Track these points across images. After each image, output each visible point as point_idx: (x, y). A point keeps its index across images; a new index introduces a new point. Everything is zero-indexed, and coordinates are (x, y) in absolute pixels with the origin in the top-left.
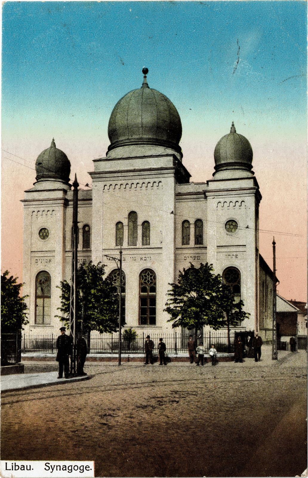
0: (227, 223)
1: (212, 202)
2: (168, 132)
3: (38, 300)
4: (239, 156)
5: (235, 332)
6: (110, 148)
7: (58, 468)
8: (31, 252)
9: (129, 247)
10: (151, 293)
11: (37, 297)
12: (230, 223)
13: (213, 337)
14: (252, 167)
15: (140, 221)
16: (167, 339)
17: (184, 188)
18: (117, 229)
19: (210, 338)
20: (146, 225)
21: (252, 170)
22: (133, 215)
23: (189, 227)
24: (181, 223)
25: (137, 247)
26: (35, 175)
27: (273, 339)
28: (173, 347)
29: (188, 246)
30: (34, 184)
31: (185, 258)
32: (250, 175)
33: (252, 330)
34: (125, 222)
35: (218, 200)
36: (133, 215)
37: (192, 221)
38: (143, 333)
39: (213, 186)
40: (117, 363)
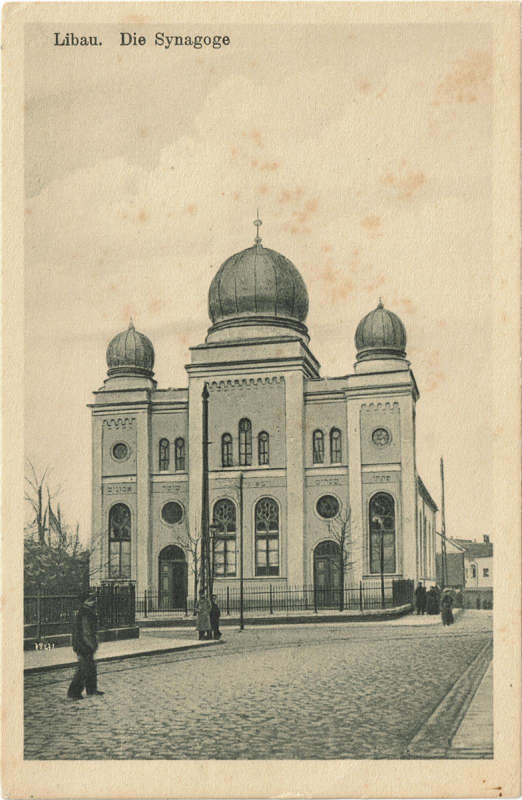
0: (373, 433)
1: (354, 406)
2: (287, 303)
3: (112, 544)
4: (384, 341)
5: (393, 581)
6: (211, 331)
7: (207, 41)
8: (136, 475)
9: (178, 472)
10: (229, 533)
11: (110, 540)
12: (379, 432)
13: (275, 591)
14: (153, 374)
15: (255, 433)
16: (365, 590)
17: (312, 387)
18: (224, 443)
19: (361, 589)
20: (263, 437)
21: (154, 378)
22: (245, 424)
23: (230, 442)
24: (157, 443)
25: (252, 467)
26: (106, 369)
27: (196, 599)
28: (238, 607)
29: (166, 472)
30: (105, 382)
31: (318, 482)
32: (403, 366)
33: (411, 579)
34: (234, 432)
35: (361, 402)
36: (245, 424)
37: (172, 440)
38: (228, 588)
39: (352, 383)
40: (238, 627)
